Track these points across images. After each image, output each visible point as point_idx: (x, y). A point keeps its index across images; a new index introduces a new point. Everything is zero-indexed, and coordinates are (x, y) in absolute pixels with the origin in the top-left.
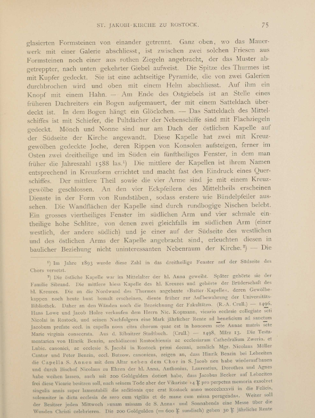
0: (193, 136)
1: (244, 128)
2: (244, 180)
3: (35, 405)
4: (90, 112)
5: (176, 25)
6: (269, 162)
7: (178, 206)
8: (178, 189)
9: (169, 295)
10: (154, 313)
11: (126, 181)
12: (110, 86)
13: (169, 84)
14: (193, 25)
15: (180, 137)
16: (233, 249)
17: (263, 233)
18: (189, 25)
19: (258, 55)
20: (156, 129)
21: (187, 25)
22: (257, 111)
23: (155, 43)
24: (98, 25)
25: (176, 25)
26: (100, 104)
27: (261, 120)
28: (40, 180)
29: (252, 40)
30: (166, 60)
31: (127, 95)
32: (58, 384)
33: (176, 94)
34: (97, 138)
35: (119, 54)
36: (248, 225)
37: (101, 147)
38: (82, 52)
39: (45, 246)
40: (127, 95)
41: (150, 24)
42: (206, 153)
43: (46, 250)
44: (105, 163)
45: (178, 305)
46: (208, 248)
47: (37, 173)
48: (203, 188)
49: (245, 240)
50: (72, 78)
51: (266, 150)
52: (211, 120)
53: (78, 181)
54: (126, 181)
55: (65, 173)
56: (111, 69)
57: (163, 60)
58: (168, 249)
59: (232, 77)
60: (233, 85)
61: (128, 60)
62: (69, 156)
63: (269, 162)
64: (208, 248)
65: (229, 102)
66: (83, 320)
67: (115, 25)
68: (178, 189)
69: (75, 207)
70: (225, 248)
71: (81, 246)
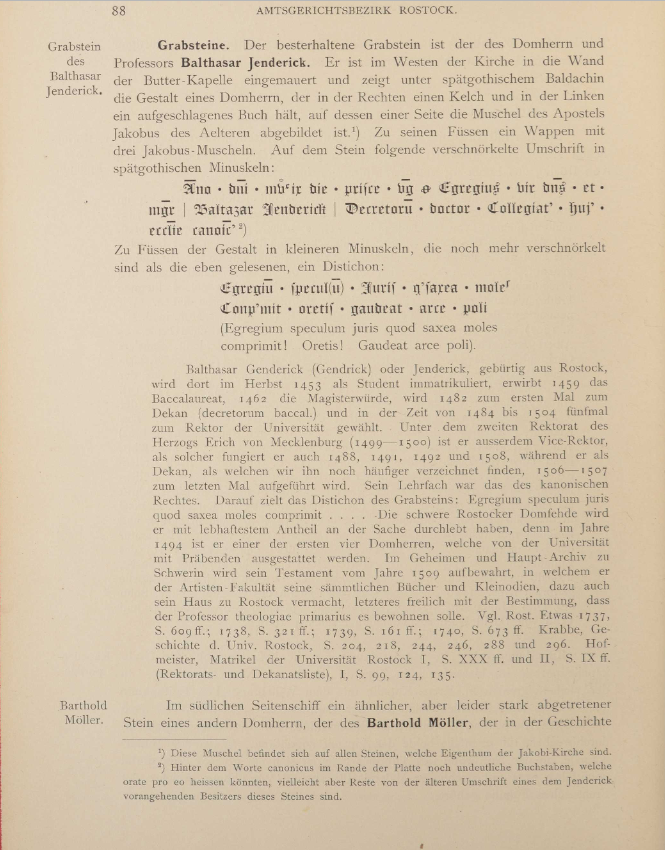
2: (279, 81)
3: (159, 588)
4: (574, 60)
5: (411, 10)
7: (498, 63)
8: (230, 724)
13: (175, 766)
14: (445, 10)
15: (196, 80)
16: (500, 63)
18: (438, 10)
21: (434, 10)
22: (360, 250)
23: (570, 705)
24: (115, 10)
25: (411, 10)
26: (512, 132)
29: (203, 147)
30: (140, 152)
31: (281, 151)
32: (546, 442)
34: (125, 152)
35: (215, 272)
36: (531, 67)
39: (499, 142)
41: (175, 766)
43: (387, 707)
44: (119, 10)
48: (210, 167)
52: (502, 97)
53: (270, 347)
56: (496, 150)
60: (281, 151)
61: (157, 169)
66: (589, 132)
67: (263, 10)
68: (230, 724)
69: (537, 132)
70: (483, 61)
71: (567, 141)
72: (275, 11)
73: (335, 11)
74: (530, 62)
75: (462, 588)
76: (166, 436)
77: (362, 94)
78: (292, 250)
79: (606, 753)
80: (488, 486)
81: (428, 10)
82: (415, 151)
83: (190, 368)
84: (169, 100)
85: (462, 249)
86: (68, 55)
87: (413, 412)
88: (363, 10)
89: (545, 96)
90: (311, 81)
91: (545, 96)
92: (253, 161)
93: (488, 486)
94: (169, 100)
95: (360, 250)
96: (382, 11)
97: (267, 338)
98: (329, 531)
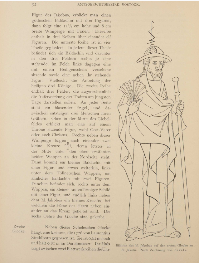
0: (56, 101)
1: (56, 32)
2: (50, 173)
3: (33, 151)
5: (126, 5)
6: (109, 97)
8: (44, 119)
9: (94, 160)
10: (95, 152)
11: (52, 75)
12: (81, 152)
17: (41, 76)
19: (103, 172)
20: (45, 211)
21: (133, 4)
22: (45, 152)
25: (126, 5)
27: (64, 114)
28: (96, 200)
31: (84, 103)
33: (45, 216)
36: (55, 66)
37: (101, 75)
38: (99, 228)
40: (85, 81)
42: (58, 90)
45: (68, 97)
46: (59, 216)
47: (83, 135)
49: (32, 97)
50: (57, 48)
51: (108, 40)
53: (34, 195)
54: (52, 75)
55: (69, 195)
57: (109, 174)
58: (46, 227)
59: (43, 249)
62: (53, 59)
63: (109, 97)
64: (59, 216)
65: (74, 249)
68: (44, 119)
72: (83, 5)
73: (102, 4)
74: (94, 43)
75: (92, 54)
76: (37, 127)
77: (79, 41)
78: (74, 201)
79: (33, 216)
80: (33, 26)
81: (131, 4)
82: (99, 37)
83: (32, 232)
84: (44, 244)
85: (105, 239)
86: (82, 99)
87: (152, 250)
88: (111, 4)
89: (71, 119)
90: (61, 48)
91: (71, 119)
92: (92, 67)
93: (33, 26)
94: (44, 244)
95: (45, 152)
96: (117, 5)
97: (77, 193)
98: (66, 157)
